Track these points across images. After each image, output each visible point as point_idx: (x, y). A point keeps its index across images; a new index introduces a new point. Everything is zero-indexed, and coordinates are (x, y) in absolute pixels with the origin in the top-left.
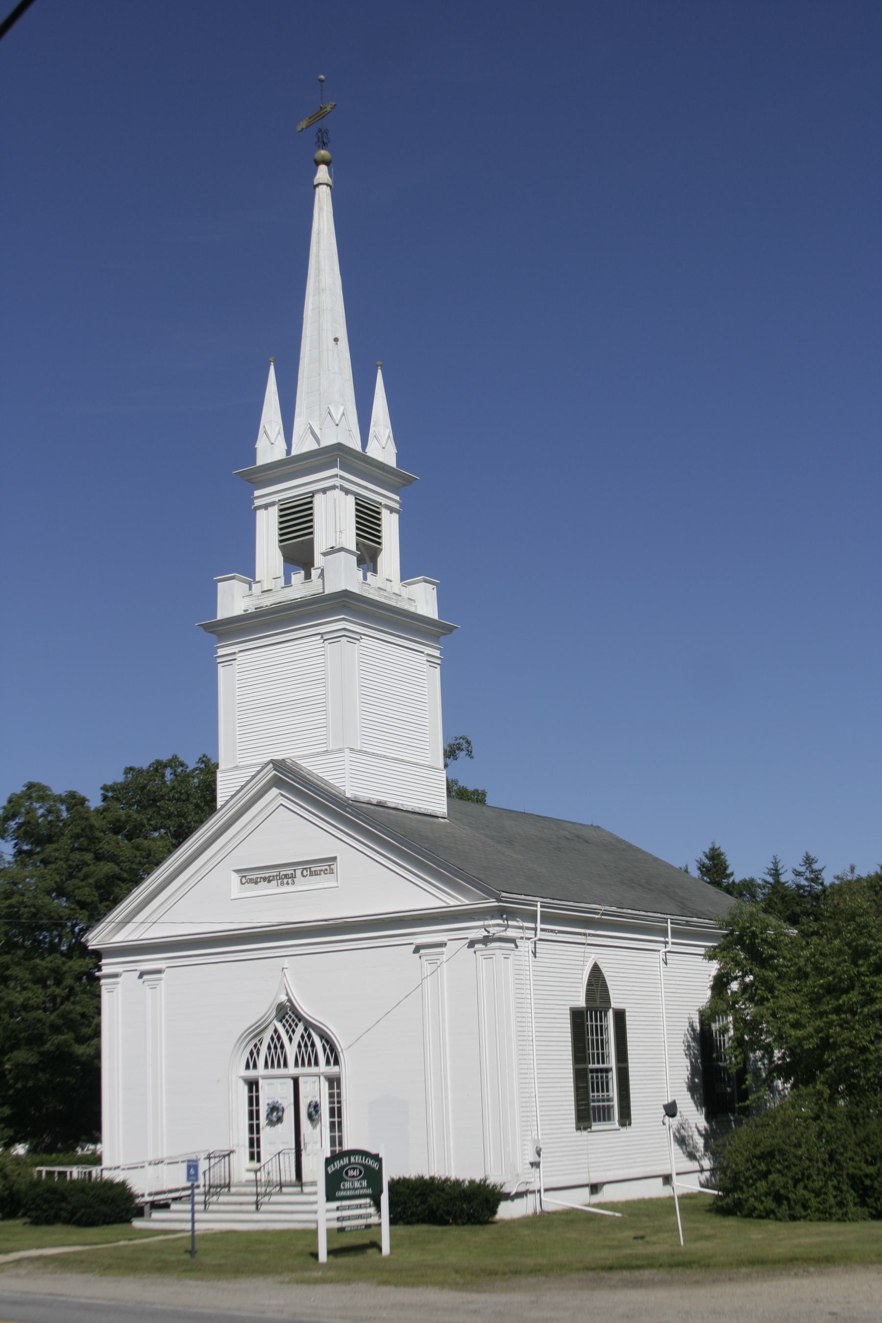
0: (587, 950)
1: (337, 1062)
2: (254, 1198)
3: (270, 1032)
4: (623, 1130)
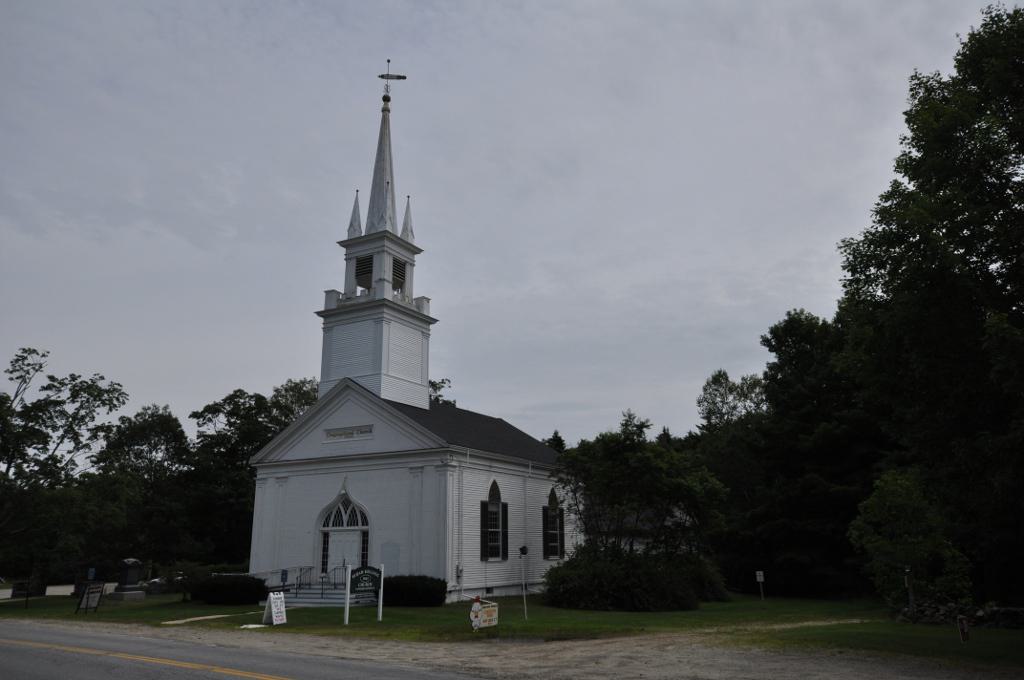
1: (367, 525)
2: (320, 592)
3: (336, 509)
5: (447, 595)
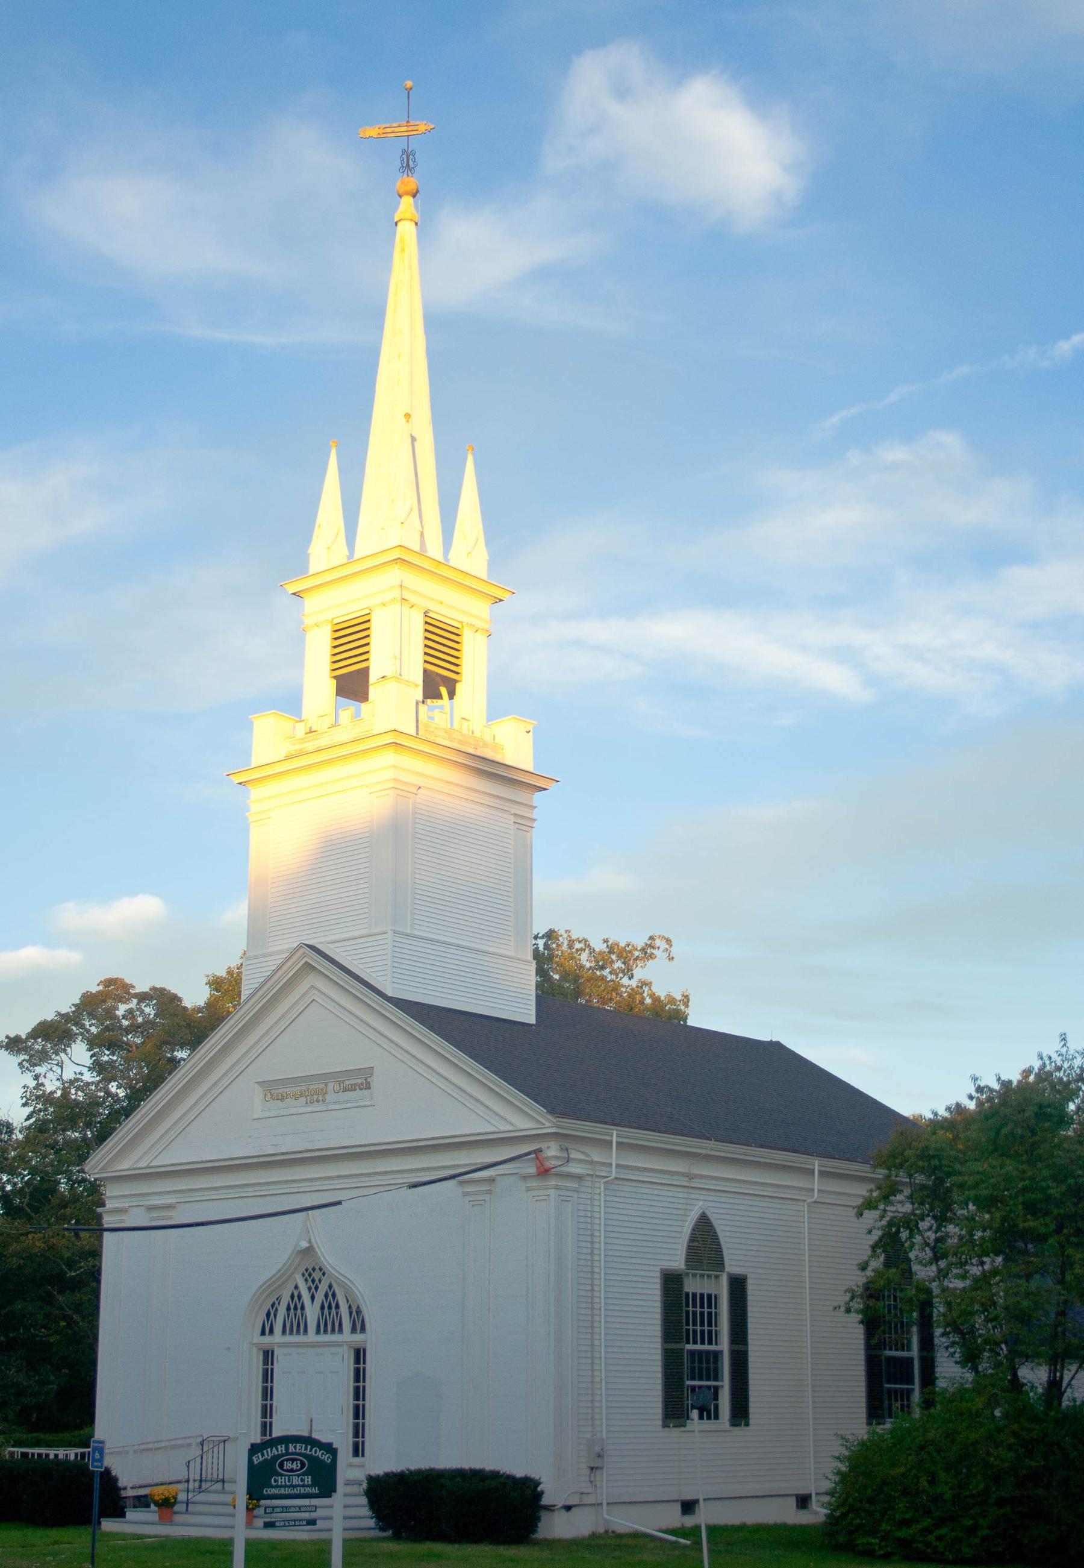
0: (692, 1196)
1: (363, 1329)
4: (738, 1431)
5: (544, 1515)
